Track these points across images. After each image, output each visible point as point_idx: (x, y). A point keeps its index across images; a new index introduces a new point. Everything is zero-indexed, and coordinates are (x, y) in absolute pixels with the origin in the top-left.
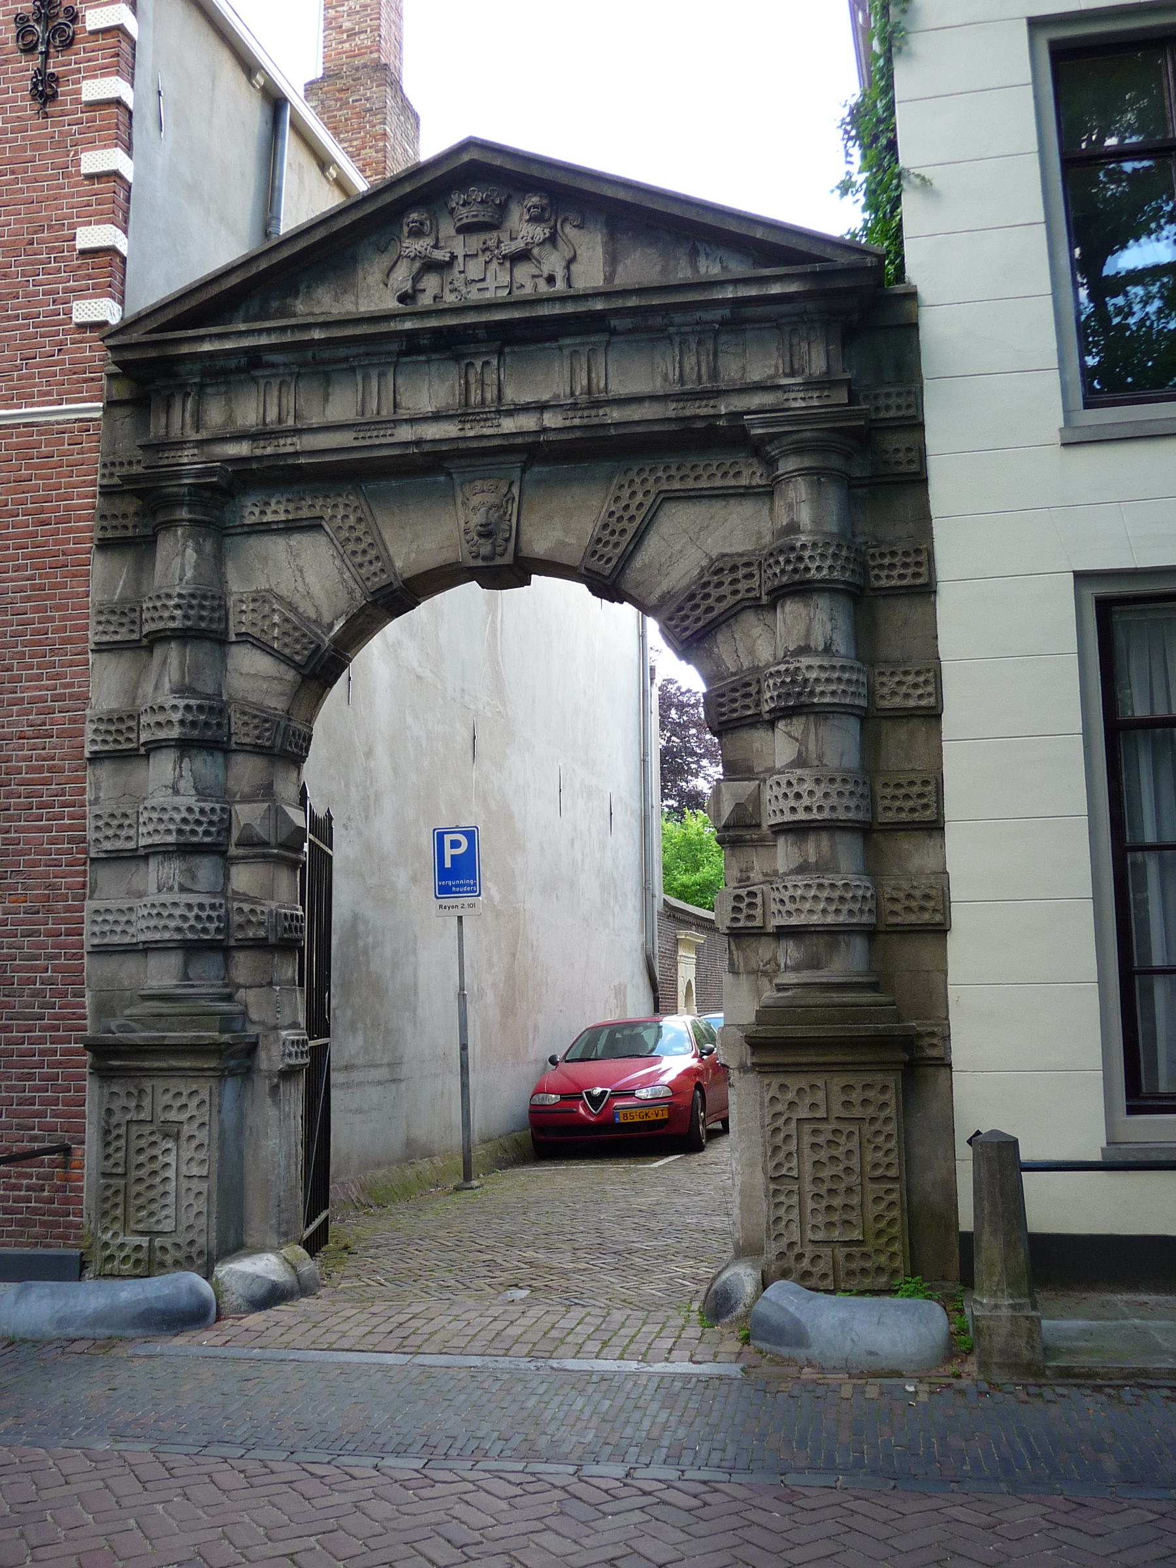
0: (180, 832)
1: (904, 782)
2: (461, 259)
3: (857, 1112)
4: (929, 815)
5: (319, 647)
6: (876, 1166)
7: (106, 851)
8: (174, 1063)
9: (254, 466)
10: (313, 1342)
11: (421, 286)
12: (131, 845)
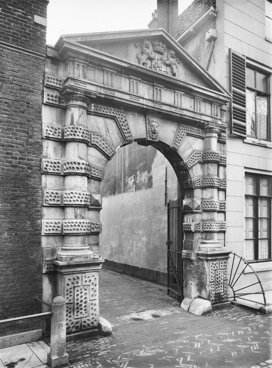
12: (59, 203)
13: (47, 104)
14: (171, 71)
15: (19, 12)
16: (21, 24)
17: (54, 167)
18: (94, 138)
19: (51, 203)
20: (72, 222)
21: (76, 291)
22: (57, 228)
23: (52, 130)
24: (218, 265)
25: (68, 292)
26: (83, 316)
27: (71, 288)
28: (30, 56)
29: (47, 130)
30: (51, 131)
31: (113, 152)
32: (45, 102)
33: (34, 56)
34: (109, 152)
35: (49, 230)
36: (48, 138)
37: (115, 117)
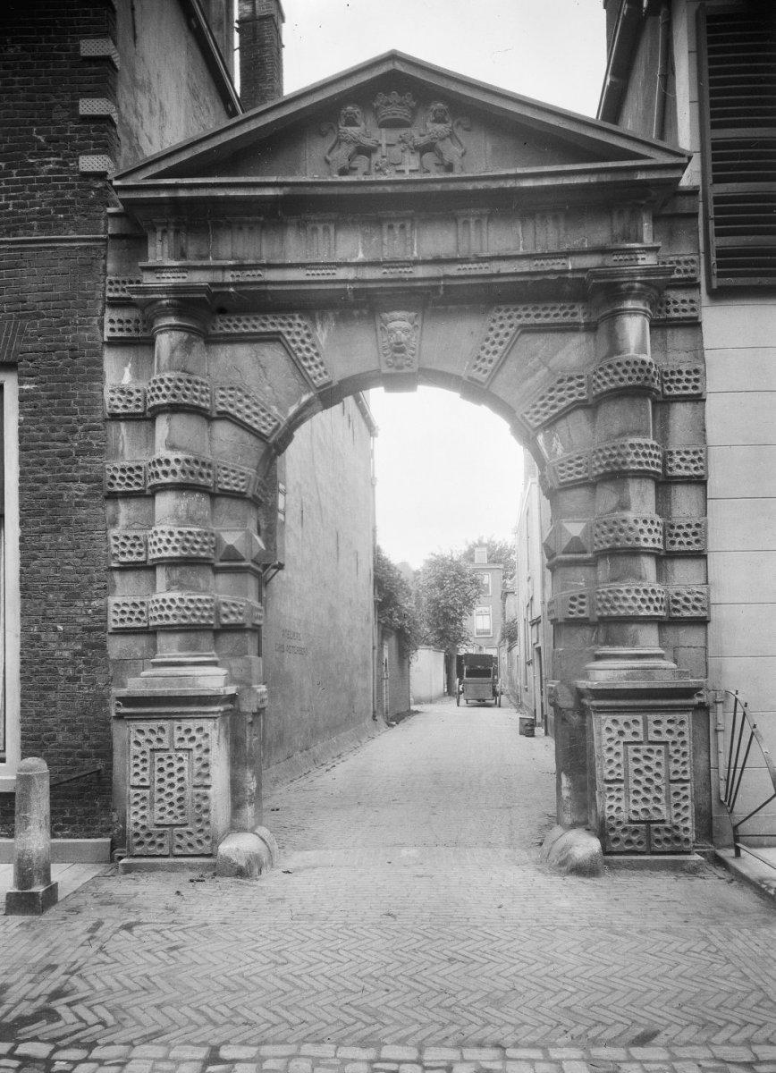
0: (668, 609)
1: (684, 525)
2: (384, 147)
3: (666, 737)
4: (696, 547)
5: (279, 424)
6: (676, 772)
7: (122, 563)
8: (157, 710)
9: (232, 290)
10: (661, 951)
11: (354, 165)
12: (142, 558)
13: (114, 343)
14: (439, 162)
15: (49, 163)
16: (55, 187)
17: (129, 478)
18: (223, 397)
19: (123, 559)
20: (164, 601)
21: (156, 759)
22: (140, 616)
23: (121, 397)
24: (639, 729)
25: (138, 761)
26: (175, 822)
27: (143, 752)
28: (74, 248)
29: (112, 399)
30: (120, 399)
31: (274, 424)
32: (106, 340)
33: (87, 244)
34: (264, 424)
35: (122, 620)
36: (115, 417)
37: (279, 333)
